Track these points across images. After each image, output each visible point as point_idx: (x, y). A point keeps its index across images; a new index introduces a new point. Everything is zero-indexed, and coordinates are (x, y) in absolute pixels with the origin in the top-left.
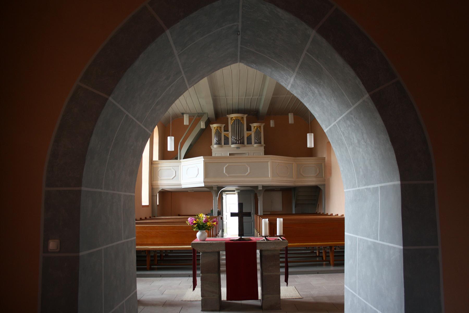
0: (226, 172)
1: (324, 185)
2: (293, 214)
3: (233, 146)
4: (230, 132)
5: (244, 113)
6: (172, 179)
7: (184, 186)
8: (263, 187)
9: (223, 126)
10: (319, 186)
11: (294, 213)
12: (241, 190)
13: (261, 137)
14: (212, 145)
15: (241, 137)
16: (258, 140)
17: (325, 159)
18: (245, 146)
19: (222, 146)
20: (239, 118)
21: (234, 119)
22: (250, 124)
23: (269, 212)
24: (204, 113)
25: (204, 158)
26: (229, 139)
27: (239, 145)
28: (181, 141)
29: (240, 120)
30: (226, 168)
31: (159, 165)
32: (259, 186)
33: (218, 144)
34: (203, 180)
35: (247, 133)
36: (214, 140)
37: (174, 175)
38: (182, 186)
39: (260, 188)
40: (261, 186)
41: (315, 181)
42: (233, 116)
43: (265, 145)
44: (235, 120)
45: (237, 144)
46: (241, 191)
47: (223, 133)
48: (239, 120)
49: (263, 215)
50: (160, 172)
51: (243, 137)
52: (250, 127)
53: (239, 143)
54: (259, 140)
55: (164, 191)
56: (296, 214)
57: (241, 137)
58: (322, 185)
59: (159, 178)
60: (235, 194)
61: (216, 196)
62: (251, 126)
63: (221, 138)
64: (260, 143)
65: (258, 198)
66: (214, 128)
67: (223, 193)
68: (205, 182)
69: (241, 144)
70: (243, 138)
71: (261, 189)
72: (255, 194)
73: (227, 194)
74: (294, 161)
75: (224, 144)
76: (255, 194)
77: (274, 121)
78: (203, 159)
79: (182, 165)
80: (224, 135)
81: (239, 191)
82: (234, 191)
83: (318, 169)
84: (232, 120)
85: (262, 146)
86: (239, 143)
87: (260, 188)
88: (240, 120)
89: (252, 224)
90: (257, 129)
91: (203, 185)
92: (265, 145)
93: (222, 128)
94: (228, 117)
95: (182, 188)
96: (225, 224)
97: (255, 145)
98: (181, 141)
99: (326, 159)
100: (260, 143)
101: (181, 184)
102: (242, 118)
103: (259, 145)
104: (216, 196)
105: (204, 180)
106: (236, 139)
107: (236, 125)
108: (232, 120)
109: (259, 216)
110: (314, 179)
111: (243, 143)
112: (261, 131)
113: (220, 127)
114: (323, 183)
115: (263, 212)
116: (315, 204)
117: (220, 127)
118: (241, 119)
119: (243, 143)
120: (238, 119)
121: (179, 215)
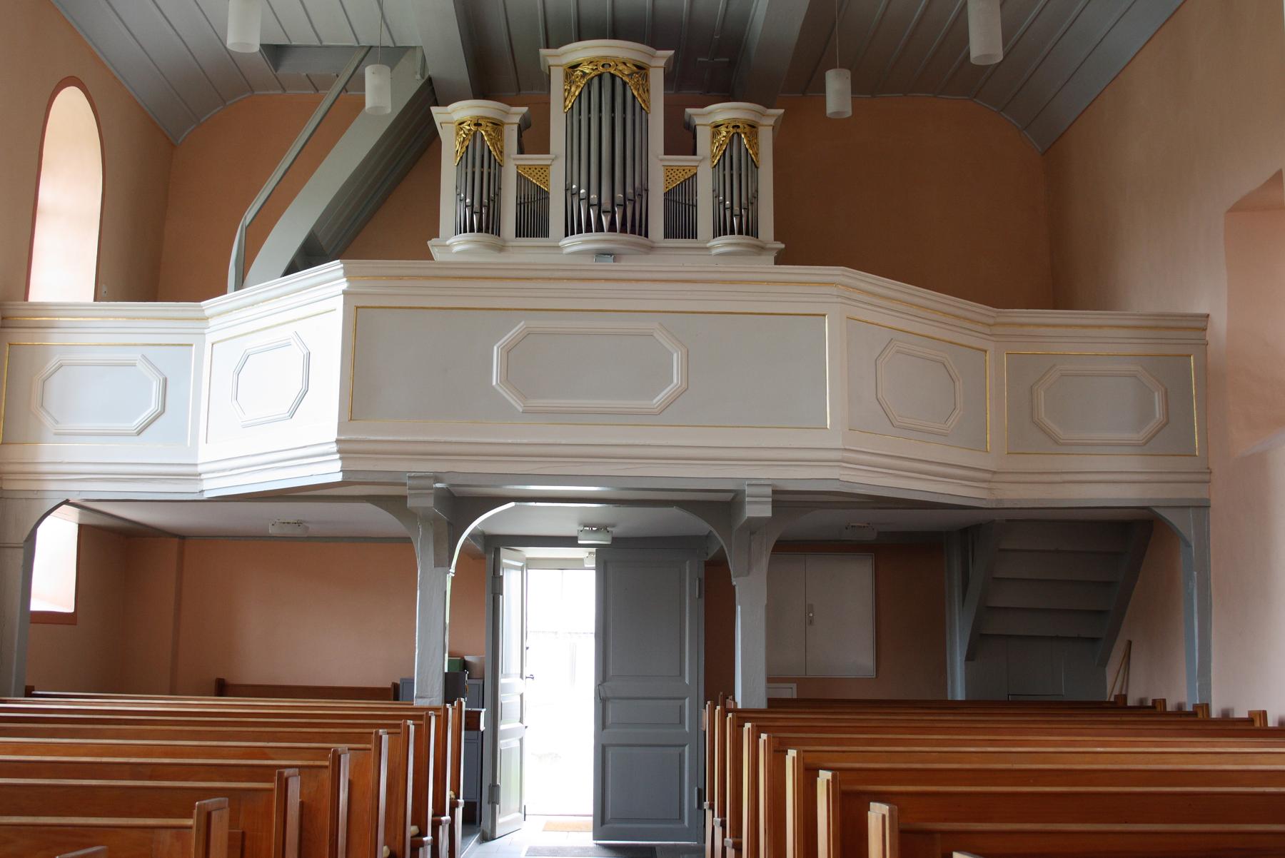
0: (507, 378)
1: (1202, 507)
2: (955, 706)
3: (575, 243)
4: (556, 157)
5: (657, 46)
6: (139, 433)
7: (215, 486)
8: (785, 501)
9: (517, 119)
10: (1165, 514)
11: (960, 695)
12: (615, 539)
13: (756, 197)
14: (437, 236)
15: (629, 190)
16: (736, 208)
17: (1205, 329)
18: (651, 249)
19: (505, 241)
20: (621, 67)
21: (584, 74)
22: (689, 111)
23: (794, 686)
24: (406, 49)
25: (347, 274)
26: (548, 198)
27: (617, 236)
28: (249, 216)
29: (624, 84)
30: (508, 351)
31: (55, 338)
32: (748, 490)
33: (480, 230)
34: (333, 435)
35: (668, 169)
36: (450, 207)
37: (153, 407)
38: (205, 485)
39: (758, 509)
40: (769, 491)
41: (1135, 477)
42: (584, 52)
43: (783, 246)
44: (596, 81)
45: (600, 228)
46: (620, 543)
47: (513, 164)
48: (618, 81)
49: (763, 705)
50: (55, 385)
51: (643, 192)
52: (691, 130)
53: (612, 228)
54: (747, 209)
55: (127, 525)
56: (977, 706)
57: (629, 190)
58: (1182, 507)
59: (48, 421)
60: (577, 564)
61: (437, 565)
62: (697, 121)
63: (498, 194)
64: (750, 229)
65: (734, 583)
66: (454, 128)
67: (503, 551)
68: (346, 449)
69: (623, 230)
70: (640, 195)
71: (766, 511)
72: (709, 564)
73: (531, 564)
74: (987, 330)
75: (519, 234)
76: (709, 564)
77: (847, 73)
78: (343, 285)
79: (209, 339)
80: (519, 175)
81: (604, 540)
82: (570, 541)
83: (1157, 398)
84: (571, 83)
85: (761, 249)
86: (612, 228)
87: (758, 509)
88: (624, 84)
89: (681, 756)
90: (734, 139)
91: (330, 471)
92: (783, 246)
93: (506, 129)
94: (551, 61)
95: (207, 495)
96: (510, 750)
97: (722, 244)
98: (249, 216)
99: (1220, 324)
100: (750, 229)
101: (200, 469)
102: (641, 69)
103: (744, 239)
104: (437, 565)
105: (340, 431)
106: (594, 197)
107: (600, 111)
108: (571, 83)
109: (760, 719)
110: (1132, 463)
111: (638, 227)
112: (756, 154)
113: (497, 125)
114: (1191, 493)
115: (770, 680)
116: (1094, 640)
117: (497, 125)
118: (630, 75)
119: (638, 227)
120: (613, 77)
121: (222, 688)
